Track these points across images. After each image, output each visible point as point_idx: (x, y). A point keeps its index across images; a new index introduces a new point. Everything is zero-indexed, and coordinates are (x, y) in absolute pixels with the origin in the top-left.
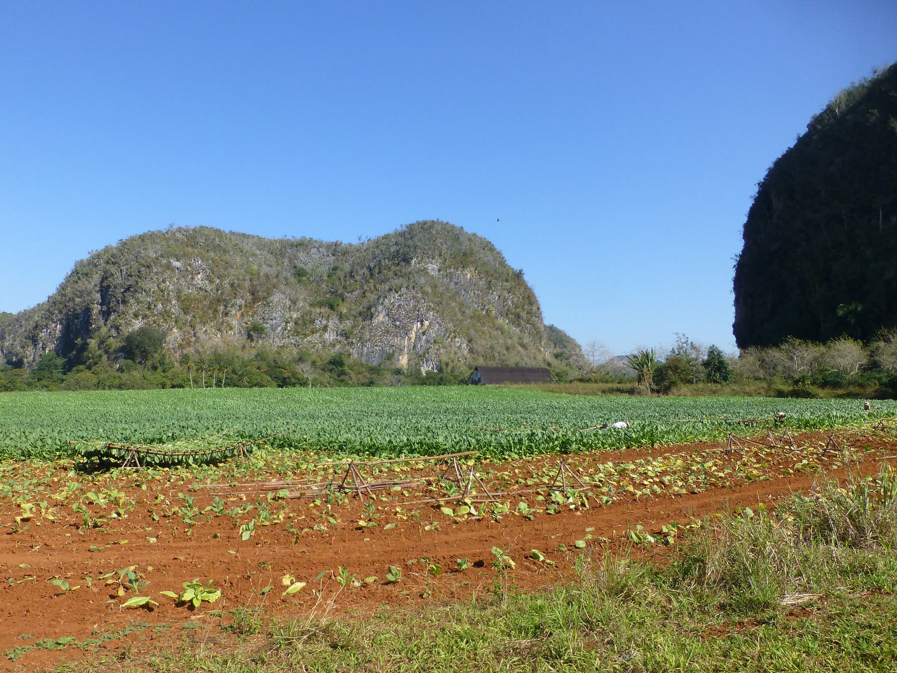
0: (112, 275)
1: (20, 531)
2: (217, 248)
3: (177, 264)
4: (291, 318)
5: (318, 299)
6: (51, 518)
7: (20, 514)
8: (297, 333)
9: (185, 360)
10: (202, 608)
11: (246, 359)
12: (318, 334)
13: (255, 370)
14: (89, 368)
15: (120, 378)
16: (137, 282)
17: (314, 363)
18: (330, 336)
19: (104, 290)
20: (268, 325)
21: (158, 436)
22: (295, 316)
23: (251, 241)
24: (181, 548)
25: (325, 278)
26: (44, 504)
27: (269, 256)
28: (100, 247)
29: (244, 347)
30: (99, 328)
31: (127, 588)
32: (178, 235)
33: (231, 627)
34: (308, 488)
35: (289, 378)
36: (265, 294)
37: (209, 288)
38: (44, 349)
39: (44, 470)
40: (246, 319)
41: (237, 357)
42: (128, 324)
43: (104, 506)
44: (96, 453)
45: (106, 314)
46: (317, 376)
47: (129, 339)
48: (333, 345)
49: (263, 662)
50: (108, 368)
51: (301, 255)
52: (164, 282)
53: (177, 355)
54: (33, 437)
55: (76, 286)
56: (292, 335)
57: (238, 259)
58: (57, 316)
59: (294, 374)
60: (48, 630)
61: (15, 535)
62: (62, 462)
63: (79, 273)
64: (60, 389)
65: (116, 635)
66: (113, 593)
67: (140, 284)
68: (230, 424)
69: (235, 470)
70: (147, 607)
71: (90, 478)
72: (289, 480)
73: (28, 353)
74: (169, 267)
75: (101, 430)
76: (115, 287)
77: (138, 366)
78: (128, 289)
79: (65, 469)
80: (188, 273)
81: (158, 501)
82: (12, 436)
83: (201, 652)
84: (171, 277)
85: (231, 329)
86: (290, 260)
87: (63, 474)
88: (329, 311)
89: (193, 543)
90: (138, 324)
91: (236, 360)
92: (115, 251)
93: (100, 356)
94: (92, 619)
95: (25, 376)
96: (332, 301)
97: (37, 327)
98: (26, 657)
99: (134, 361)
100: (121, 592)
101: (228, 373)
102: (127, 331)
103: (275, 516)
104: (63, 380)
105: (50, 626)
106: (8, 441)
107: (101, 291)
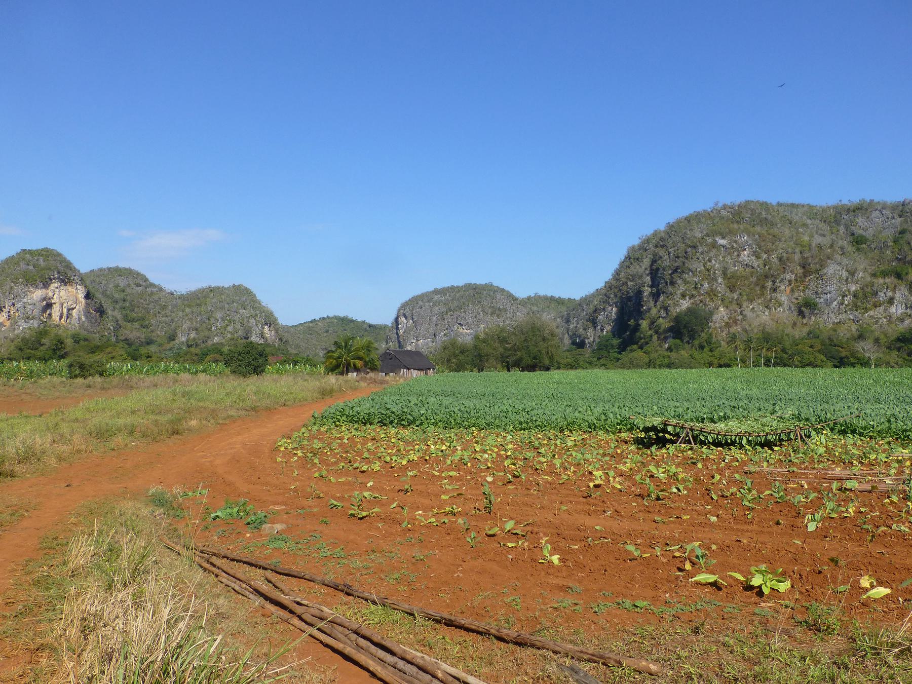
0: (661, 258)
1: (594, 496)
2: (764, 222)
3: (723, 242)
4: (849, 291)
5: (882, 268)
6: (619, 487)
7: (592, 480)
8: (856, 307)
9: (733, 339)
10: (770, 596)
11: (797, 337)
12: (882, 308)
13: (807, 349)
14: (641, 348)
15: (669, 357)
16: (684, 263)
17: (877, 341)
18: (897, 310)
19: (654, 273)
20: (822, 300)
21: (709, 416)
22: (853, 288)
23: (800, 210)
24: (742, 530)
25: (890, 243)
26: (612, 473)
27: (822, 225)
28: (649, 232)
29: (795, 324)
30: (649, 309)
31: (693, 564)
32: (724, 213)
33: (806, 622)
34: (880, 481)
35: (847, 357)
36: (818, 266)
37: (755, 264)
38: (602, 330)
39: (607, 442)
40: (796, 294)
41: (787, 335)
42: (676, 305)
43: (664, 481)
44: (654, 429)
45: (656, 296)
46: (881, 356)
47: (677, 319)
48: (902, 320)
49: (846, 667)
50: (658, 348)
51: (860, 220)
52: (710, 260)
53: (724, 334)
54: (599, 410)
55: (629, 271)
56: (851, 310)
57: (787, 232)
59: (853, 354)
60: (624, 590)
61: (589, 499)
62: (622, 435)
63: (632, 258)
64: (616, 367)
65: (688, 608)
66: (680, 565)
68: (784, 407)
69: (792, 455)
70: (714, 584)
71: (649, 452)
72: (856, 470)
74: (714, 245)
75: (655, 407)
76: (664, 270)
77: (686, 345)
78: (675, 271)
79: (626, 442)
80: (734, 250)
81: (715, 480)
82: (580, 409)
83: (776, 642)
84: (716, 256)
85: (780, 306)
86: (846, 227)
87: (625, 447)
88: (896, 281)
89: (755, 527)
90: (685, 304)
91: (786, 338)
92: (663, 234)
93: (651, 336)
94: (663, 588)
95: (587, 356)
96: (899, 269)
97: (596, 310)
98: (609, 614)
99: (682, 341)
100: (688, 566)
101: (777, 352)
102: (675, 311)
103: (844, 509)
104: (619, 359)
105: (627, 587)
106: (577, 414)
107: (651, 274)
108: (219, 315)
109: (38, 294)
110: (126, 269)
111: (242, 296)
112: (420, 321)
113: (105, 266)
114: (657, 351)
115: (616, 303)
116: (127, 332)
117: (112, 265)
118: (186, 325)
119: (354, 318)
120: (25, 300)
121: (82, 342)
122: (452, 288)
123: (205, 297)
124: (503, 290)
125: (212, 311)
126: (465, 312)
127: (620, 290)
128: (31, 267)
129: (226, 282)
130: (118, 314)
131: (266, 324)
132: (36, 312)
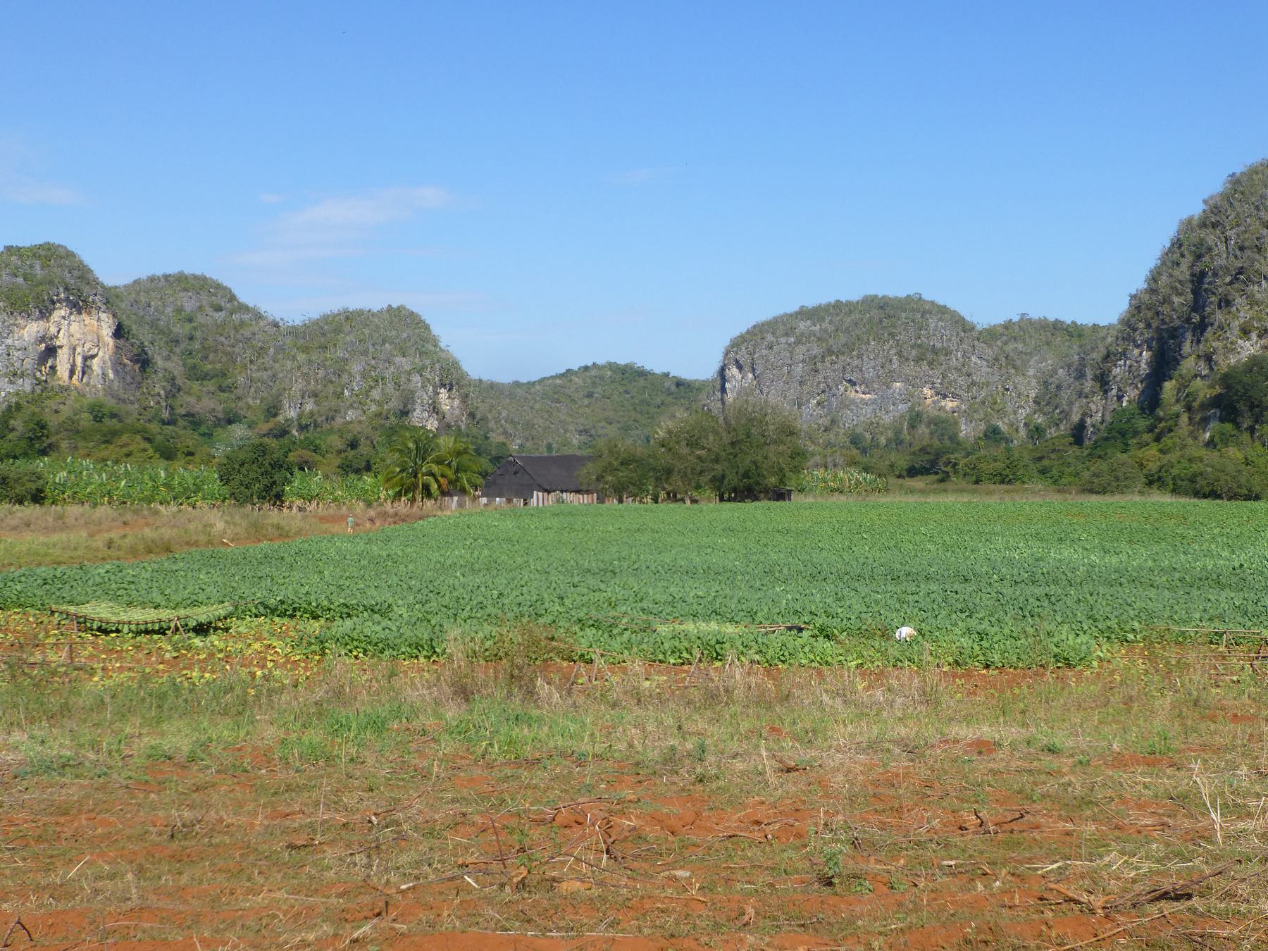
0: (1210, 249)
38: (1120, 398)
47: (1226, 380)
50: (1190, 441)
58: (1143, 334)
67: (1257, 265)
73: (1093, 407)
76: (1215, 275)
90: (1249, 348)
93: (1178, 416)
97: (1108, 356)
99: (1237, 426)
108: (356, 367)
109: (31, 330)
110: (195, 277)
111: (405, 330)
112: (768, 375)
113: (159, 272)
114: (1183, 447)
115: (1148, 342)
116: (192, 400)
117: (172, 269)
118: (298, 387)
119: (648, 368)
120: (9, 341)
121: (107, 421)
122: (838, 305)
123: (338, 331)
124: (943, 310)
125: (345, 360)
126: (860, 356)
127: (1158, 313)
128: (20, 280)
129: (374, 301)
130: (176, 367)
131: (443, 385)
132: (29, 364)
